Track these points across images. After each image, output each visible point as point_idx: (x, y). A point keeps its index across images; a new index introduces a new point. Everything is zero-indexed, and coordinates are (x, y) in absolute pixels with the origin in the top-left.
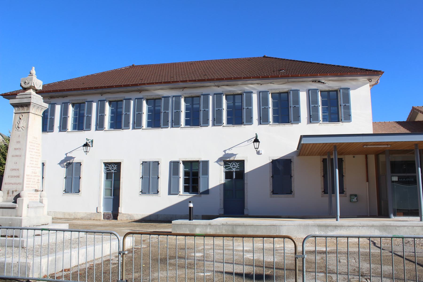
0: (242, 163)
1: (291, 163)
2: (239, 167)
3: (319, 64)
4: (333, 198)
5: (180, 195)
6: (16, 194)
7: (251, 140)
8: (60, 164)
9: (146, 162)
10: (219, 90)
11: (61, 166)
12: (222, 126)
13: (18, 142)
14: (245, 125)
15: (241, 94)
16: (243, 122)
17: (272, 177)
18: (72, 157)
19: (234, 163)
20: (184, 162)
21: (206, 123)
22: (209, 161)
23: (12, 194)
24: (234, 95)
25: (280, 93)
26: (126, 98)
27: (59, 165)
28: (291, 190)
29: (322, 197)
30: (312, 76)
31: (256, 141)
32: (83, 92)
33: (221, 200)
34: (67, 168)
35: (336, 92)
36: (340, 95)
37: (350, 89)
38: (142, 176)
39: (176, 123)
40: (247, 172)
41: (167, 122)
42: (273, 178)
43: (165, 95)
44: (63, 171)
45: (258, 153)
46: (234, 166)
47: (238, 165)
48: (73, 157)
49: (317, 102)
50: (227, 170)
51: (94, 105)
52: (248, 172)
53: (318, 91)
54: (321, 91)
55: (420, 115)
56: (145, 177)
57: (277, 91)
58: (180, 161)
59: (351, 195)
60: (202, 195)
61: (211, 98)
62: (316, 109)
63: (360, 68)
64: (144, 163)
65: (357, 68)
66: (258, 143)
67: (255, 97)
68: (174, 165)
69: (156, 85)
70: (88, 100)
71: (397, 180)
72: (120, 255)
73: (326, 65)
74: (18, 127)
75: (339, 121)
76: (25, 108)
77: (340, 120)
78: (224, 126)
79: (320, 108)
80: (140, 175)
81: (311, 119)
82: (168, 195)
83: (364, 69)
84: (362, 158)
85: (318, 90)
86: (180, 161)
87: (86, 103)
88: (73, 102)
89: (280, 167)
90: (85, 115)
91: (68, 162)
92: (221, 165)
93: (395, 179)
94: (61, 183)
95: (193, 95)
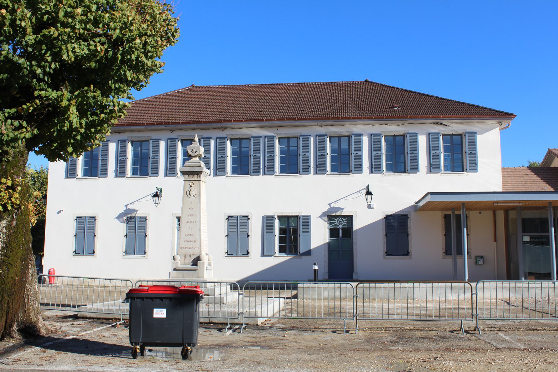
0: (350, 218)
1: (407, 219)
2: (346, 224)
3: (438, 98)
4: (459, 261)
5: (275, 256)
6: (193, 257)
7: (361, 191)
8: (118, 218)
9: (81, 217)
10: (322, 130)
11: (119, 221)
12: (326, 174)
13: (190, 209)
14: (353, 174)
15: (349, 137)
16: (351, 170)
17: (385, 235)
18: (134, 210)
19: (340, 219)
20: (280, 217)
21: (306, 170)
22: (310, 215)
23: (189, 258)
24: (340, 137)
25: (394, 136)
26: (204, 136)
27: (116, 219)
28: (408, 251)
29: (443, 259)
30: (434, 117)
31: (369, 193)
32: (148, 127)
33: (325, 262)
34: (127, 223)
35: (460, 136)
36: (465, 140)
37: (477, 133)
38: (228, 234)
39: (269, 170)
40: (357, 230)
41: (259, 168)
42: (387, 237)
43: (254, 135)
44: (122, 227)
45: (369, 207)
46: (340, 222)
47: (345, 220)
48: (342, 207)
49: (438, 148)
50: (332, 227)
51: (162, 144)
52: (357, 229)
53: (439, 135)
54: (443, 135)
55: (556, 158)
56: (232, 234)
57: (393, 134)
58: (275, 216)
59: (476, 257)
60: (303, 257)
61: (312, 140)
62: (437, 156)
63: (489, 109)
64: (229, 218)
65: (485, 108)
66: (370, 196)
67: (365, 140)
68: (268, 221)
69: (245, 123)
70: (153, 138)
71: (529, 240)
72: (287, 311)
73: (448, 100)
74: (189, 194)
75: (463, 171)
76: (195, 176)
77: (465, 169)
78: (328, 175)
79: (442, 156)
80: (225, 232)
81: (432, 168)
82: (261, 256)
83: (493, 110)
84: (490, 213)
85: (440, 133)
86: (275, 216)
87: (151, 141)
88: (133, 139)
89: (395, 224)
90: (151, 156)
91: (129, 216)
92: (326, 221)
93: (527, 239)
94: (121, 243)
95: (290, 136)
